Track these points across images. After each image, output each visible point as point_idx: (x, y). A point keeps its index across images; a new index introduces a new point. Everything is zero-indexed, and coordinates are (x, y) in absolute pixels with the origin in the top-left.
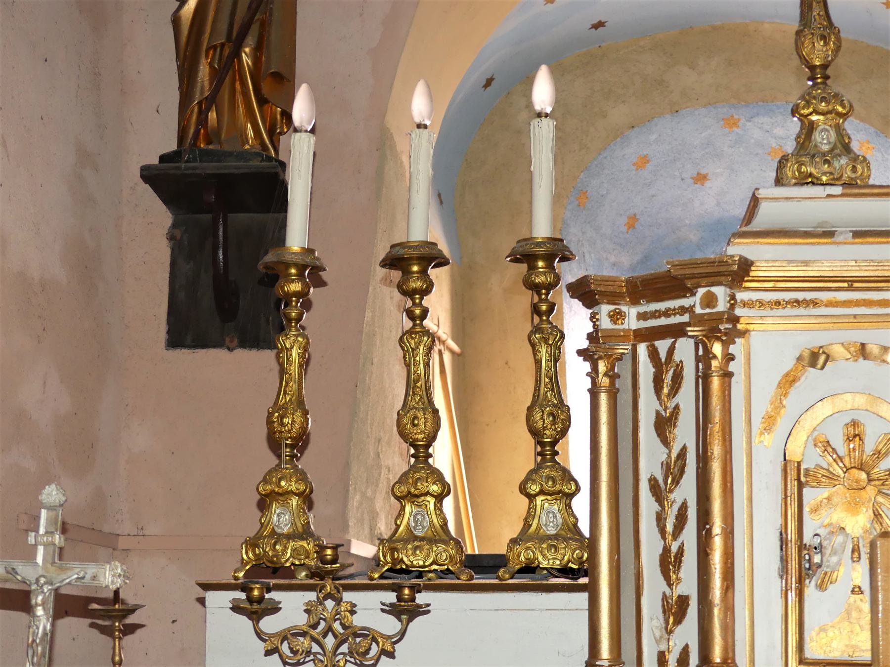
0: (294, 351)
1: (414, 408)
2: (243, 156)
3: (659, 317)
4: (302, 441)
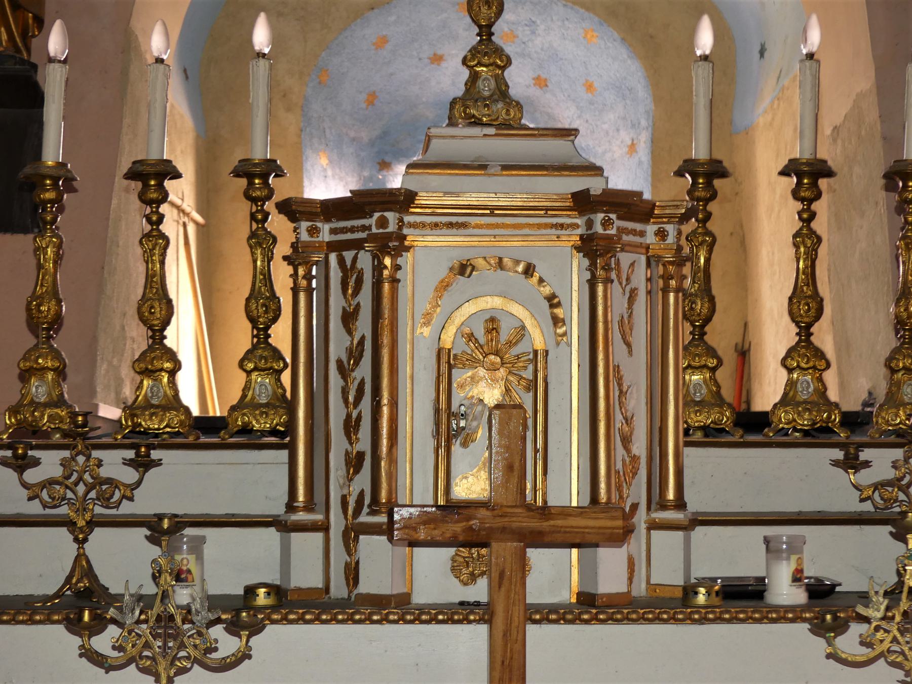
0: (49, 250)
1: (151, 299)
3: (346, 232)
4: (57, 322)
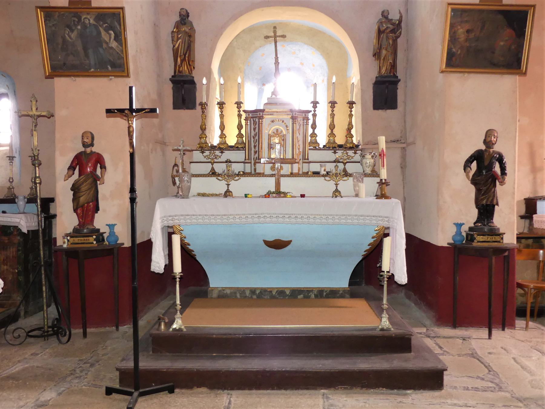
2: (187, 76)
